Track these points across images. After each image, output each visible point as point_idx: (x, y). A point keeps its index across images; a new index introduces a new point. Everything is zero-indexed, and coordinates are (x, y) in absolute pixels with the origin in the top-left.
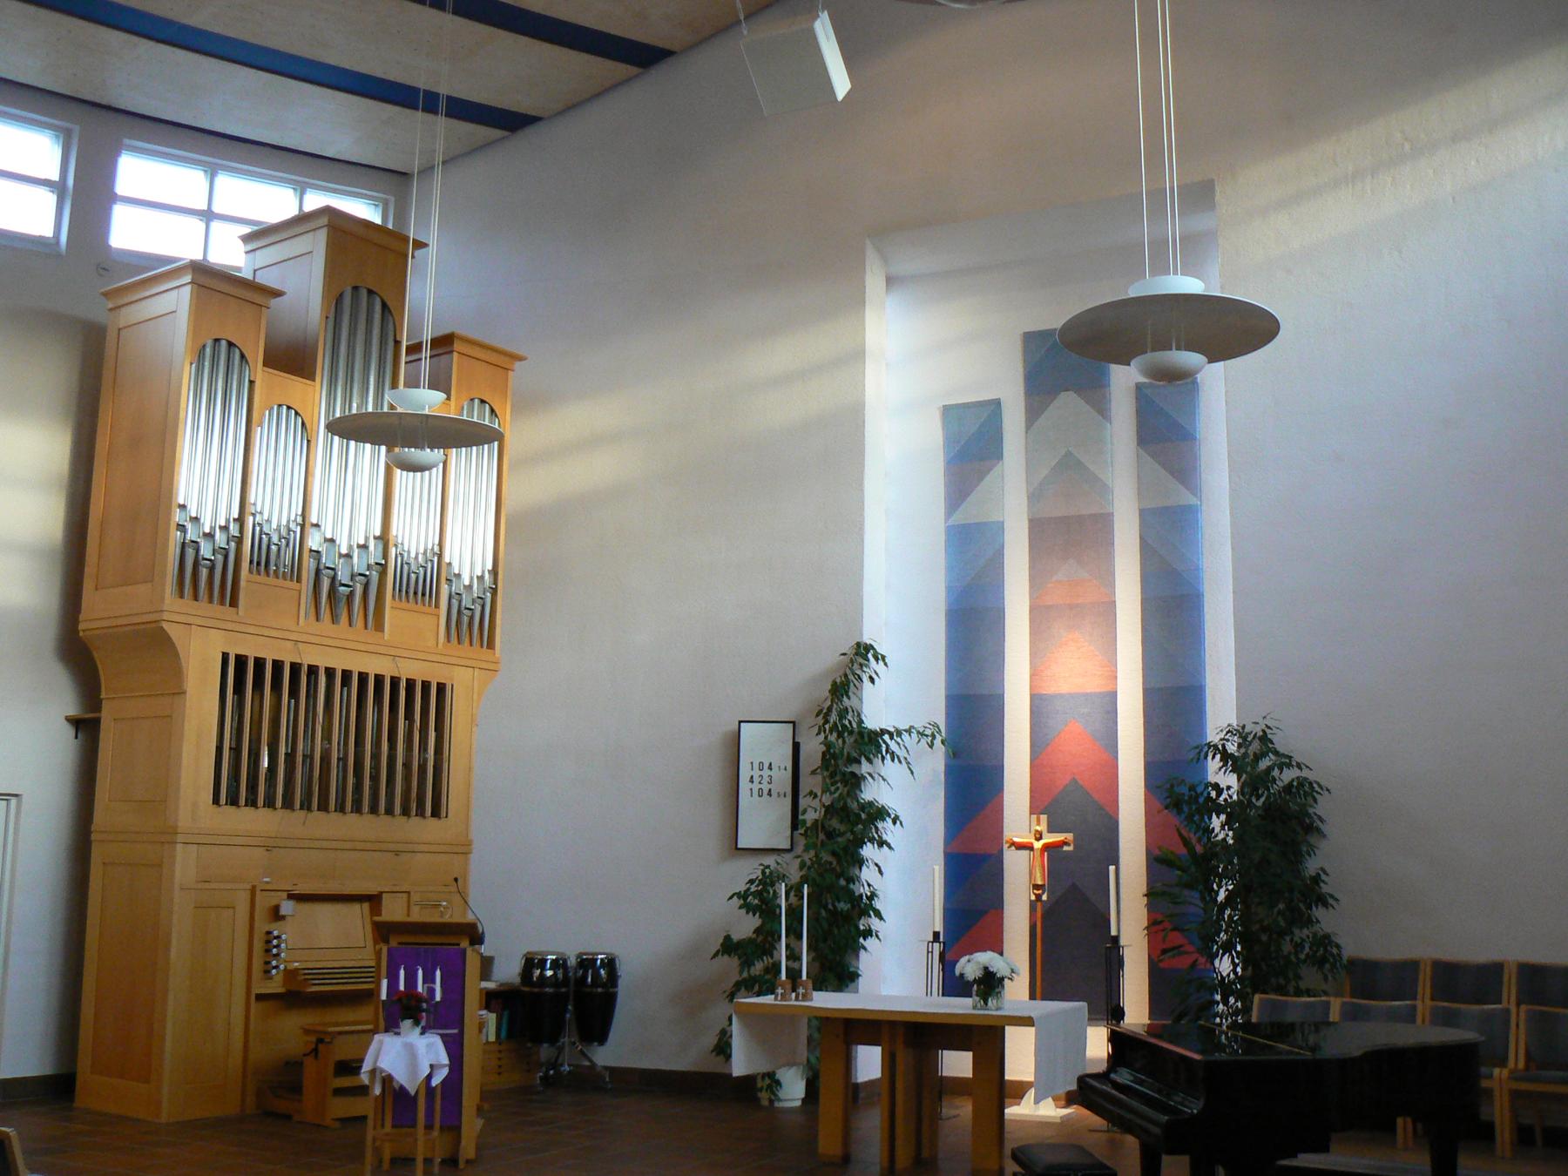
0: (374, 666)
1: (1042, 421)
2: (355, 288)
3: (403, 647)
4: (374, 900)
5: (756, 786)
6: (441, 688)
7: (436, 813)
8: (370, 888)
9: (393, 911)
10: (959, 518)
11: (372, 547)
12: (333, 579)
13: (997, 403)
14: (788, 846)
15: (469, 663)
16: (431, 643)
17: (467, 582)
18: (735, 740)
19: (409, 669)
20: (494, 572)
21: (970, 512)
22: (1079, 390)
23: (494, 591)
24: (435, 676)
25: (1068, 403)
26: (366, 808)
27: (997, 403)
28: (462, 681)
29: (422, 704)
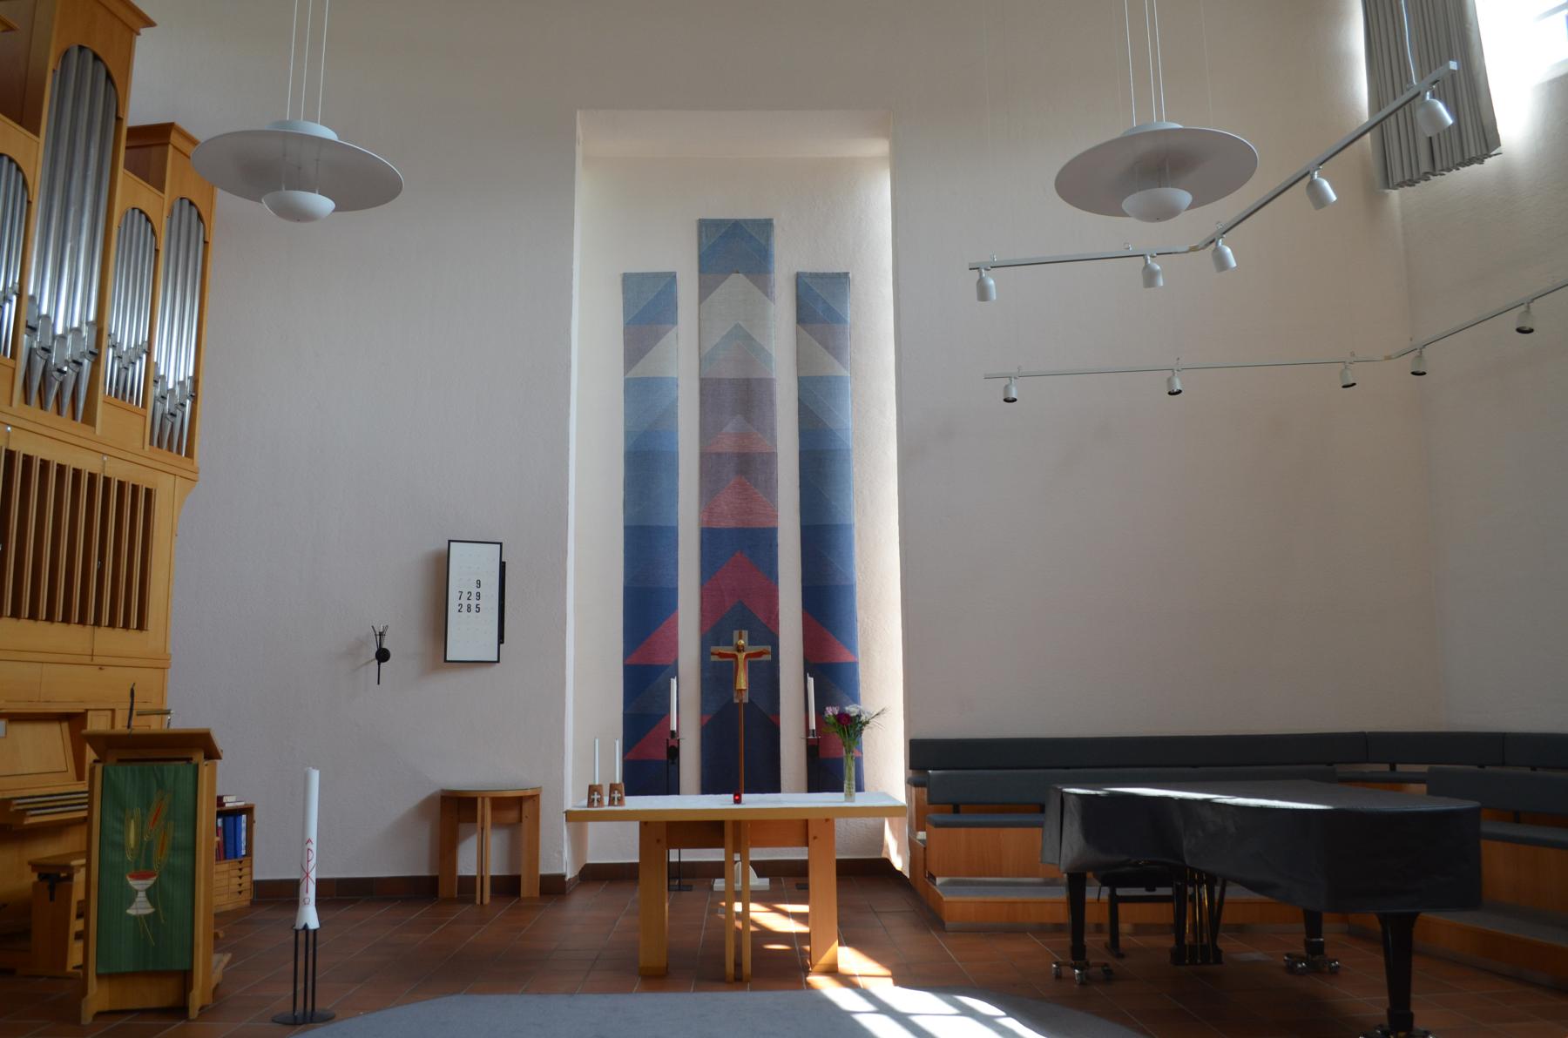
0: (88, 463)
1: (715, 296)
2: (81, 48)
3: (105, 449)
4: (75, 719)
5: (465, 602)
6: (149, 492)
7: (141, 626)
8: (79, 708)
9: (97, 724)
10: (631, 375)
11: (85, 334)
12: (47, 362)
13: (671, 278)
14: (452, 655)
15: (173, 470)
16: (138, 444)
17: (170, 386)
18: (442, 564)
19: (118, 471)
20: (195, 380)
21: (639, 371)
22: (748, 273)
23: (194, 398)
24: (143, 478)
25: (736, 283)
26: (26, 610)
27: (671, 278)
28: (165, 489)
29: (129, 510)
